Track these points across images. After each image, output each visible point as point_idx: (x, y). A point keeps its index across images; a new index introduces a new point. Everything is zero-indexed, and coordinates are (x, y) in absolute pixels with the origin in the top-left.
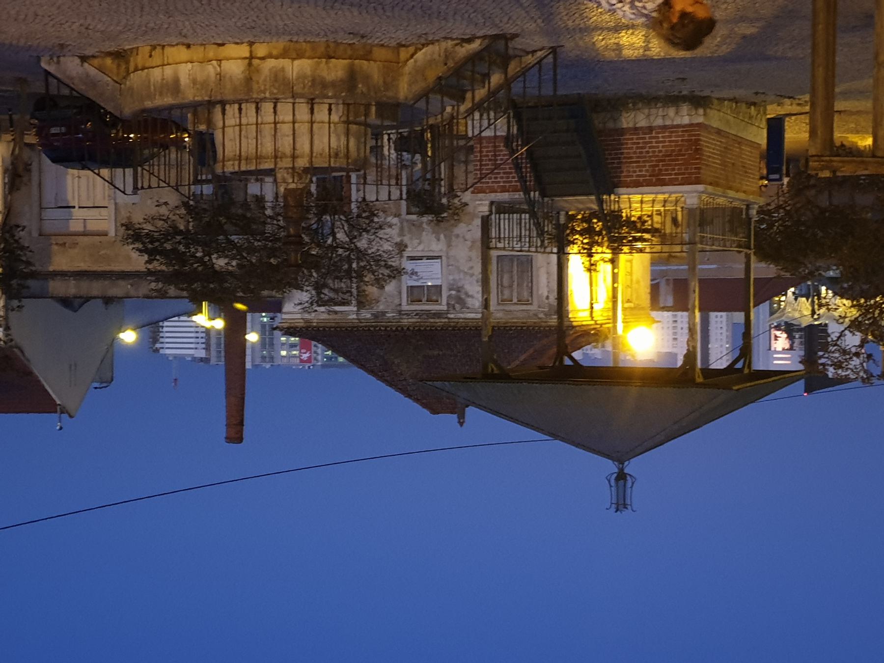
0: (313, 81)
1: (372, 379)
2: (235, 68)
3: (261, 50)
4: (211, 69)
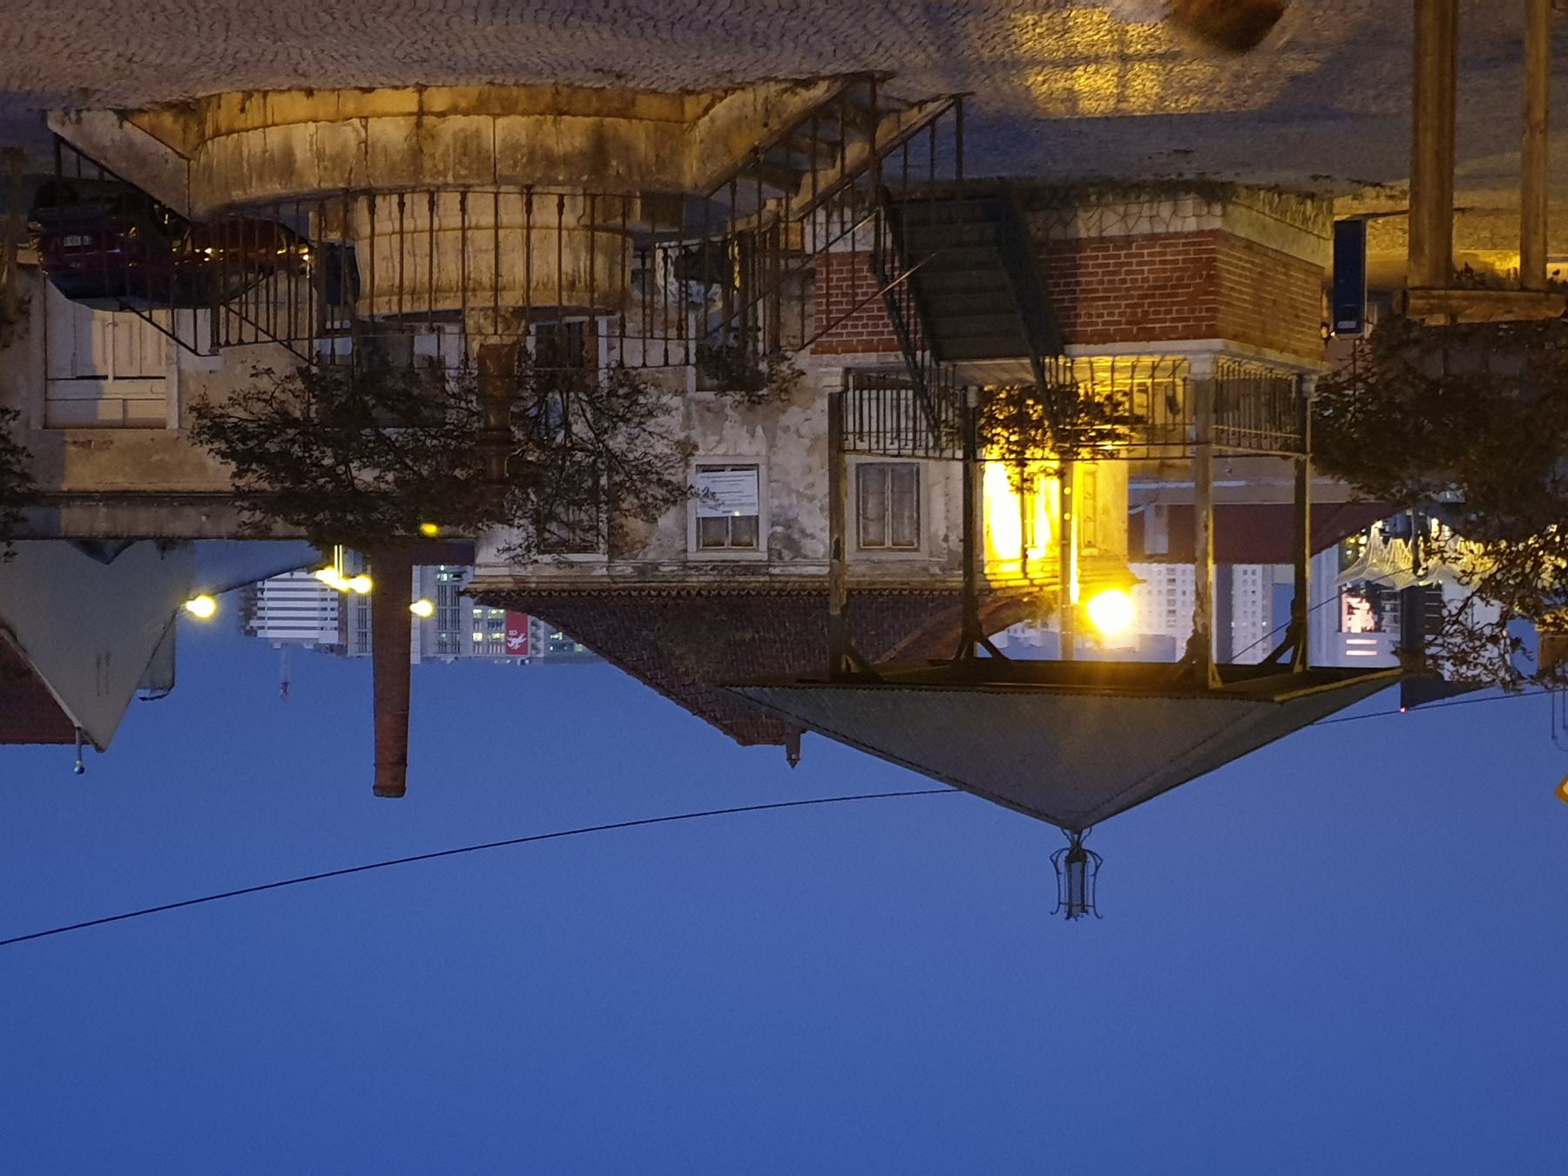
0: (532, 153)
2: (392, 132)
3: (438, 100)
4: (350, 134)
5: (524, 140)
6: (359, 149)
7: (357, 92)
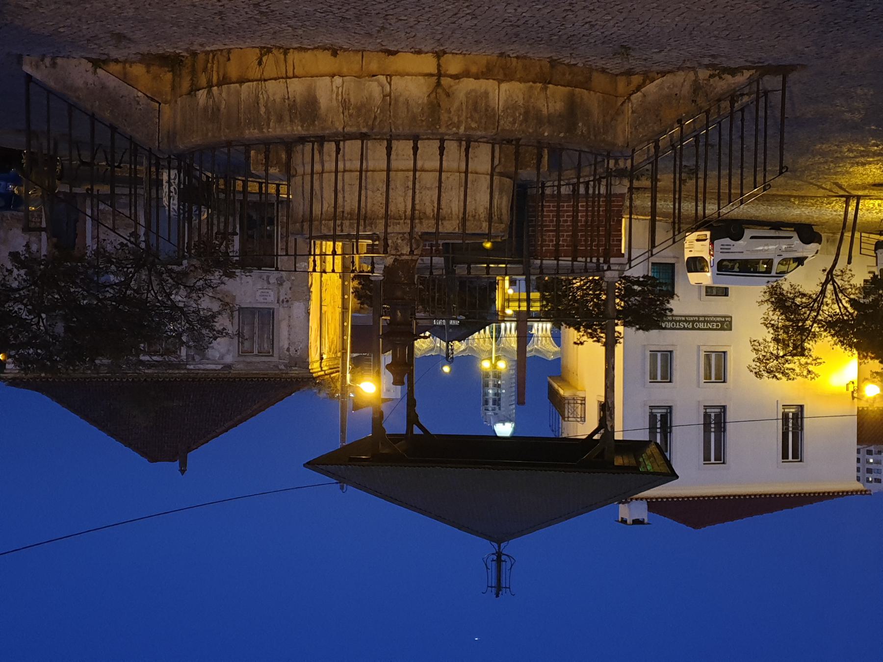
0: (527, 112)
1: (94, 429)
3: (454, 65)
4: (374, 88)
5: (521, 102)
6: (384, 100)
7: (382, 55)
